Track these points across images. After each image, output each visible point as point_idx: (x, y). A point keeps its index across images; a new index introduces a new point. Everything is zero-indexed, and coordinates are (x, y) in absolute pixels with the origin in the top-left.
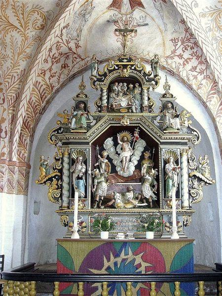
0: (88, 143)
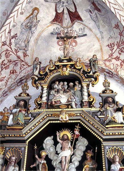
0: (24, 141)
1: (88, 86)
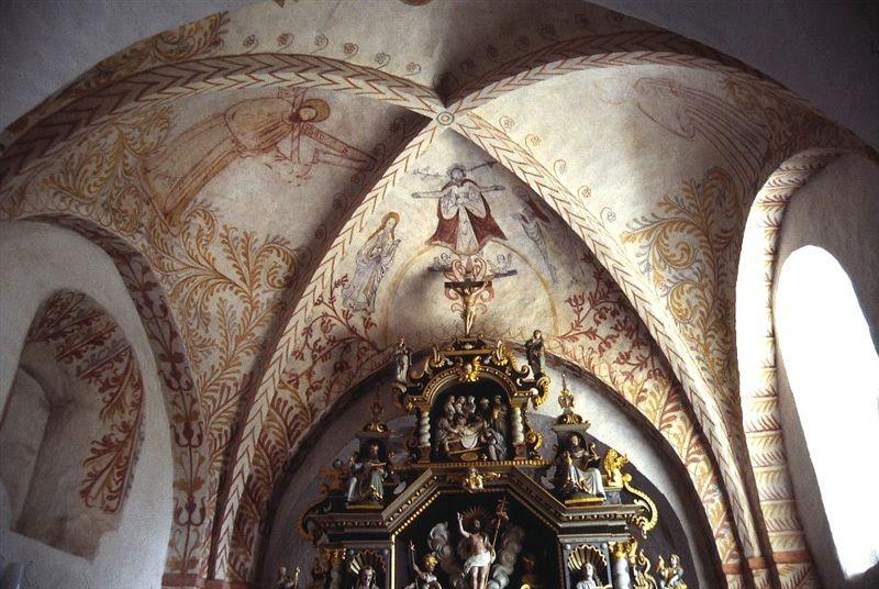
1: (524, 406)
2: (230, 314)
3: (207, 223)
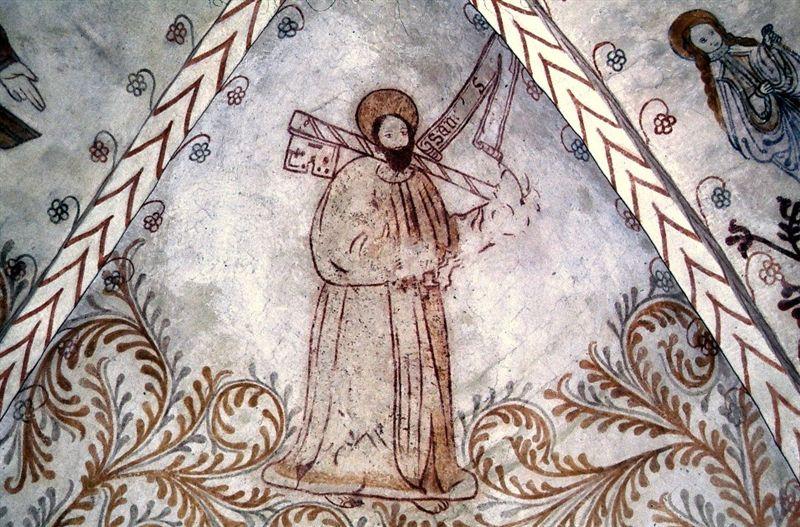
2: (695, 512)
3: (518, 423)
